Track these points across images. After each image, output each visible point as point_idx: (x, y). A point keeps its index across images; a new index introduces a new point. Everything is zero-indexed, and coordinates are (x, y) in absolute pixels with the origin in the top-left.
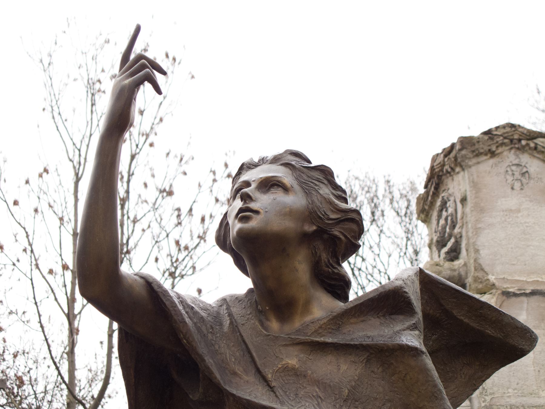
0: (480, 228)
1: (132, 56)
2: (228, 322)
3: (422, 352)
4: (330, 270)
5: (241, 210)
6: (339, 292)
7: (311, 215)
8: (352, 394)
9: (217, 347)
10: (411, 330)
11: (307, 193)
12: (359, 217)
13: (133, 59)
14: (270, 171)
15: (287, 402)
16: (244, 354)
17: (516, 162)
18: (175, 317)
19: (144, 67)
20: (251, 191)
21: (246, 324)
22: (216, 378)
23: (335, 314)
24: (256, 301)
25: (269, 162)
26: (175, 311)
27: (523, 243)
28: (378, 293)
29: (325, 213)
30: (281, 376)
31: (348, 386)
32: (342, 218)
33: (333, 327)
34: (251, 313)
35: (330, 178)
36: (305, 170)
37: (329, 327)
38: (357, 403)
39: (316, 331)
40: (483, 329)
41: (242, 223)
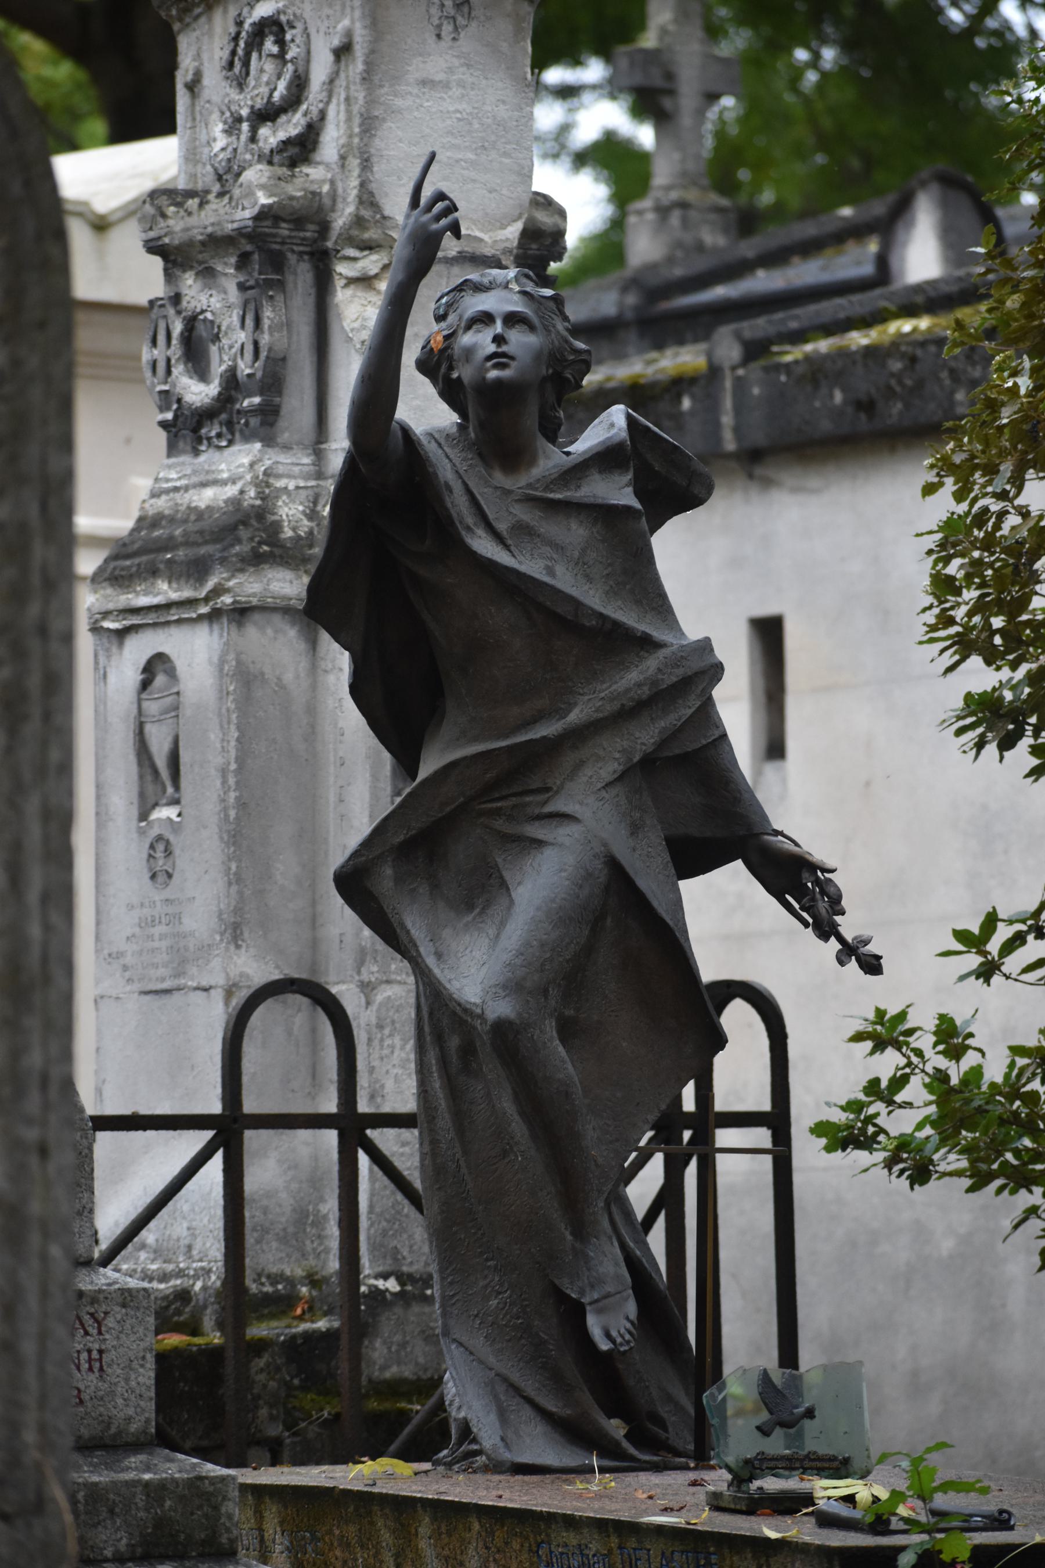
0: (377, 117)
1: (427, 193)
14: (509, 301)
27: (448, 154)
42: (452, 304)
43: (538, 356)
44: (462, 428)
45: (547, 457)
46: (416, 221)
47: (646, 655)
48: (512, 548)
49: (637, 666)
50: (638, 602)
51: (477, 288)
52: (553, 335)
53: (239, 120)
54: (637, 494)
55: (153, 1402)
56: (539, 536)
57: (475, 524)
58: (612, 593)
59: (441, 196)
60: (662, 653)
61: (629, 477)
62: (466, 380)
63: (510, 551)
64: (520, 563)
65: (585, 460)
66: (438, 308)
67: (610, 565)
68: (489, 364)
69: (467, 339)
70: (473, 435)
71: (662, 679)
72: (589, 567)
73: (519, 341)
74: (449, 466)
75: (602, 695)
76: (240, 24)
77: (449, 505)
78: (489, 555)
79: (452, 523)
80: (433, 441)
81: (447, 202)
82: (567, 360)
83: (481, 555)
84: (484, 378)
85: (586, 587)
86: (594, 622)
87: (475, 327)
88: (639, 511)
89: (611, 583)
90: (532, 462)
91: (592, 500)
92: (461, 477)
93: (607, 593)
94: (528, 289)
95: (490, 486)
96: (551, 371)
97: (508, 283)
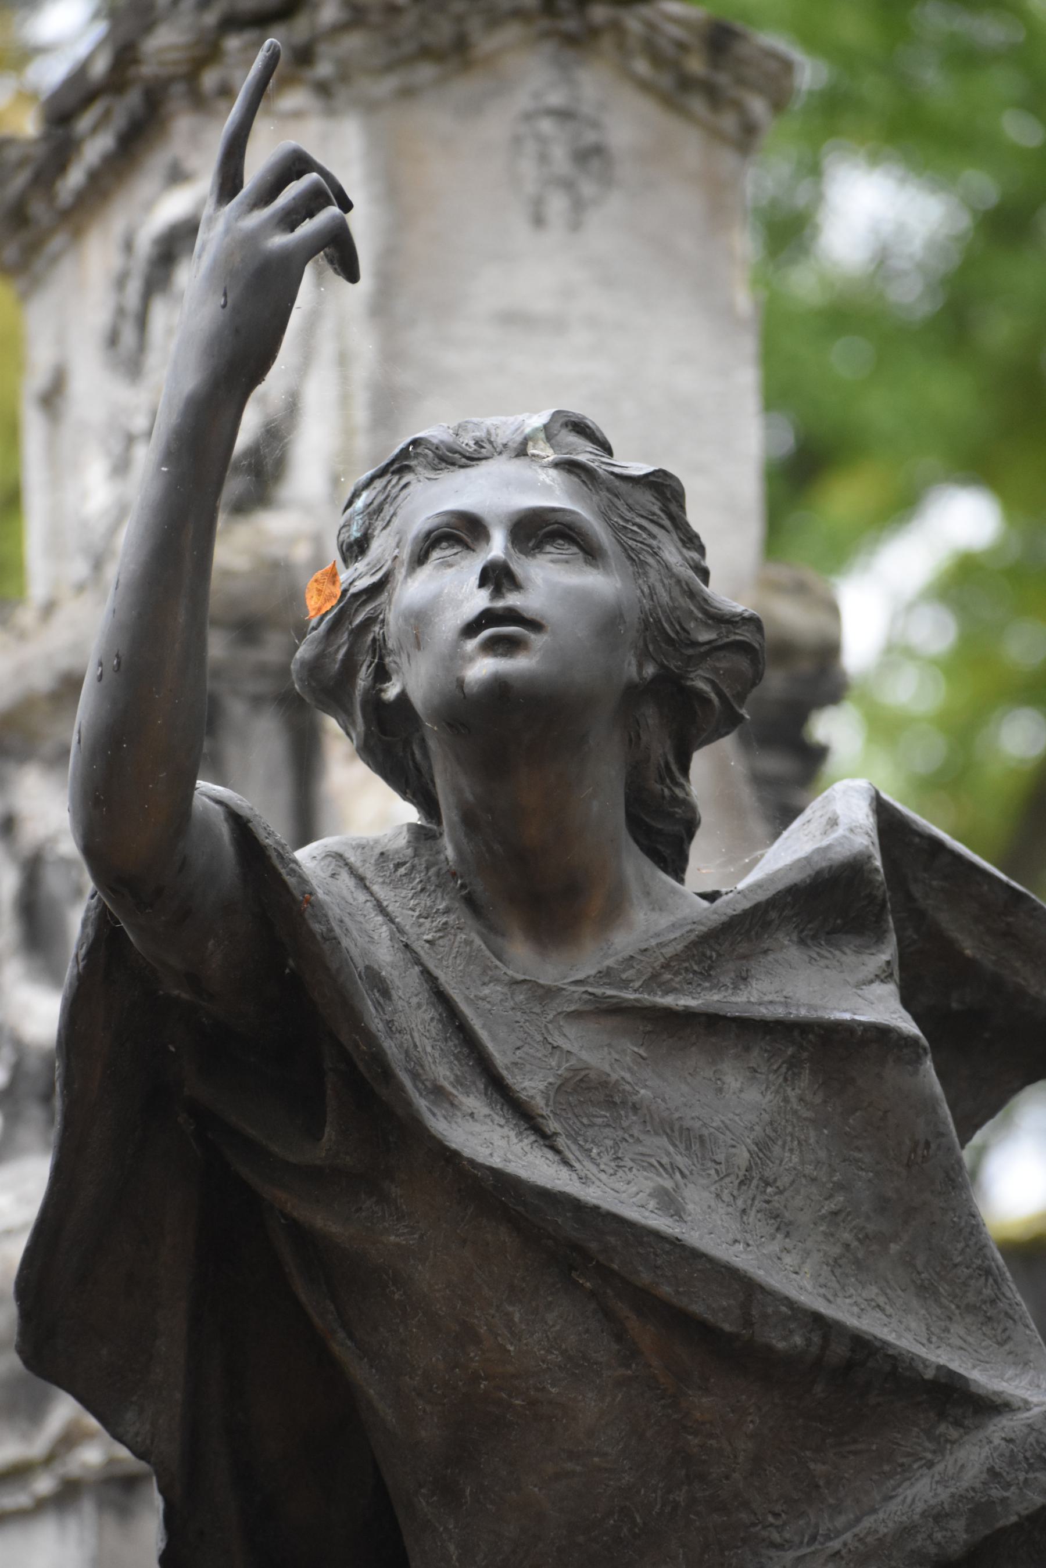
4: (666, 792)
5: (486, 618)
6: (666, 852)
10: (882, 981)
12: (758, 637)
14: (529, 486)
17: (556, 99)
21: (441, 942)
23: (704, 929)
28: (812, 873)
30: (570, 1104)
32: (720, 643)
33: (696, 968)
34: (447, 911)
35: (673, 508)
36: (617, 483)
37: (686, 964)
38: (769, 1190)
39: (654, 976)
42: (380, 510)
43: (609, 624)
44: (422, 837)
45: (658, 906)
46: (227, 230)
47: (954, 1433)
48: (561, 1142)
49: (930, 1465)
50: (925, 1291)
51: (442, 459)
52: (653, 576)
53: (130, 440)
54: (907, 1002)
56: (635, 1108)
57: (458, 1082)
58: (851, 1264)
59: (297, 164)
60: (999, 1428)
61: (885, 957)
62: (418, 698)
63: (557, 1151)
64: (584, 1180)
65: (757, 907)
66: (347, 525)
67: (840, 1187)
68: (471, 645)
69: (414, 589)
70: (450, 852)
71: (1004, 1500)
72: (780, 1192)
73: (549, 582)
74: (384, 931)
75: (836, 1545)
76: (128, 246)
77: (376, 1024)
78: (496, 1162)
79: (387, 1074)
80: (344, 875)
81: (314, 176)
82: (695, 644)
83: (472, 1162)
84: (460, 683)
85: (774, 1247)
86: (798, 1340)
87: (435, 554)
88: (913, 1041)
89: (847, 1236)
90: (614, 910)
91: (779, 1012)
92: (418, 961)
93: (835, 1264)
94: (582, 458)
95: (497, 980)
96: (650, 670)
97: (525, 442)
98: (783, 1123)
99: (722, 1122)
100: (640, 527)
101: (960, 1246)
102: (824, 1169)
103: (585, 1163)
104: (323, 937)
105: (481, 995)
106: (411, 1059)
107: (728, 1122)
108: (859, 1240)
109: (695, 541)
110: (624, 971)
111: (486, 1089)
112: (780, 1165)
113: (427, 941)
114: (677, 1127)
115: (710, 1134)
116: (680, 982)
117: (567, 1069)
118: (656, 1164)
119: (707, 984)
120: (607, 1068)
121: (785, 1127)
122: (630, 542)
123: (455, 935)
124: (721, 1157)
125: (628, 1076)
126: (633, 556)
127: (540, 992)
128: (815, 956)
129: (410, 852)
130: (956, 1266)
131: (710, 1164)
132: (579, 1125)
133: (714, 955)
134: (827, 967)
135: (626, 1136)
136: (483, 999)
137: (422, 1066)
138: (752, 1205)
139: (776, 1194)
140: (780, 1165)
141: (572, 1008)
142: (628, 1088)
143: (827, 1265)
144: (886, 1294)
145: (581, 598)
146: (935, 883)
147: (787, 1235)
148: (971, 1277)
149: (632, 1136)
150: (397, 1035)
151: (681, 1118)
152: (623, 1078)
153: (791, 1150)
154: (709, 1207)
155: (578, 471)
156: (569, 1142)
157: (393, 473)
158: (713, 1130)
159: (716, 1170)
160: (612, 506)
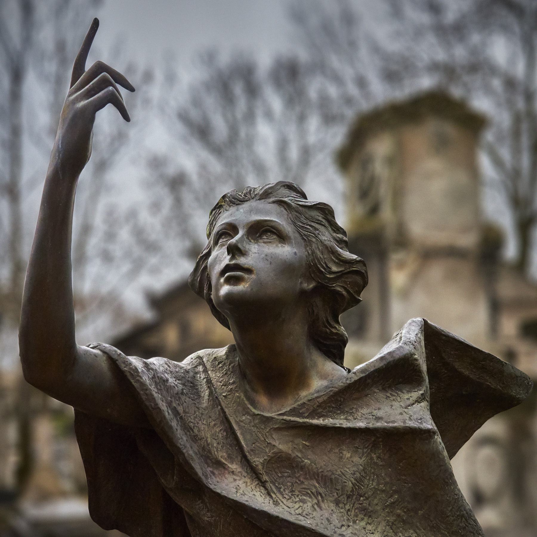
1: (89, 65)
2: (207, 392)
3: (434, 433)
4: (328, 330)
5: (228, 268)
6: (335, 351)
7: (312, 269)
8: (356, 489)
9: (196, 430)
11: (306, 241)
13: (90, 69)
14: (258, 211)
15: (283, 502)
16: (227, 435)
18: (148, 403)
19: (105, 83)
20: (241, 240)
21: (229, 397)
22: (196, 474)
24: (239, 364)
25: (258, 197)
26: (147, 395)
29: (327, 265)
30: (273, 467)
31: (352, 479)
32: (346, 271)
33: (334, 406)
34: (233, 383)
35: (330, 217)
36: (301, 208)
37: (329, 405)
38: (362, 498)
40: (483, 381)
41: (230, 285)
43: (287, 269)
48: (269, 485)
52: (314, 246)
55: (402, 424)
59: (100, 67)
63: (266, 489)
64: (276, 503)
67: (395, 492)
72: (367, 499)
90: (302, 380)
98: (370, 468)
99: (341, 471)
100: (310, 226)
101: (450, 509)
102: (388, 486)
103: (278, 494)
104: (152, 408)
105: (242, 420)
106: (205, 451)
107: (343, 472)
108: (405, 512)
109: (340, 230)
110: (301, 409)
111: (241, 459)
112: (367, 487)
113: (224, 396)
114: (320, 475)
115: (335, 478)
116: (326, 412)
117: (273, 453)
118: (309, 492)
119: (339, 412)
120: (290, 452)
121: (371, 470)
122: (304, 232)
123: (235, 394)
124: (339, 487)
125: (300, 455)
126: (305, 238)
127: (264, 419)
128: (388, 395)
129: (224, 357)
130: (448, 516)
131: (334, 491)
132: (277, 477)
133: (342, 399)
134: (394, 400)
135: (297, 481)
136: (242, 422)
137: (211, 454)
138: (353, 507)
139: (364, 500)
140: (367, 487)
141: (277, 426)
142: (299, 460)
143: (389, 526)
144: (416, 533)
145: (269, 259)
146: (452, 352)
147: (370, 516)
148: (454, 520)
149: (299, 480)
150: (199, 441)
151: (322, 471)
152: (297, 456)
153: (373, 480)
154: (332, 510)
155: (283, 204)
156: (271, 485)
157: (218, 208)
158: (336, 476)
159: (337, 493)
160: (297, 218)
